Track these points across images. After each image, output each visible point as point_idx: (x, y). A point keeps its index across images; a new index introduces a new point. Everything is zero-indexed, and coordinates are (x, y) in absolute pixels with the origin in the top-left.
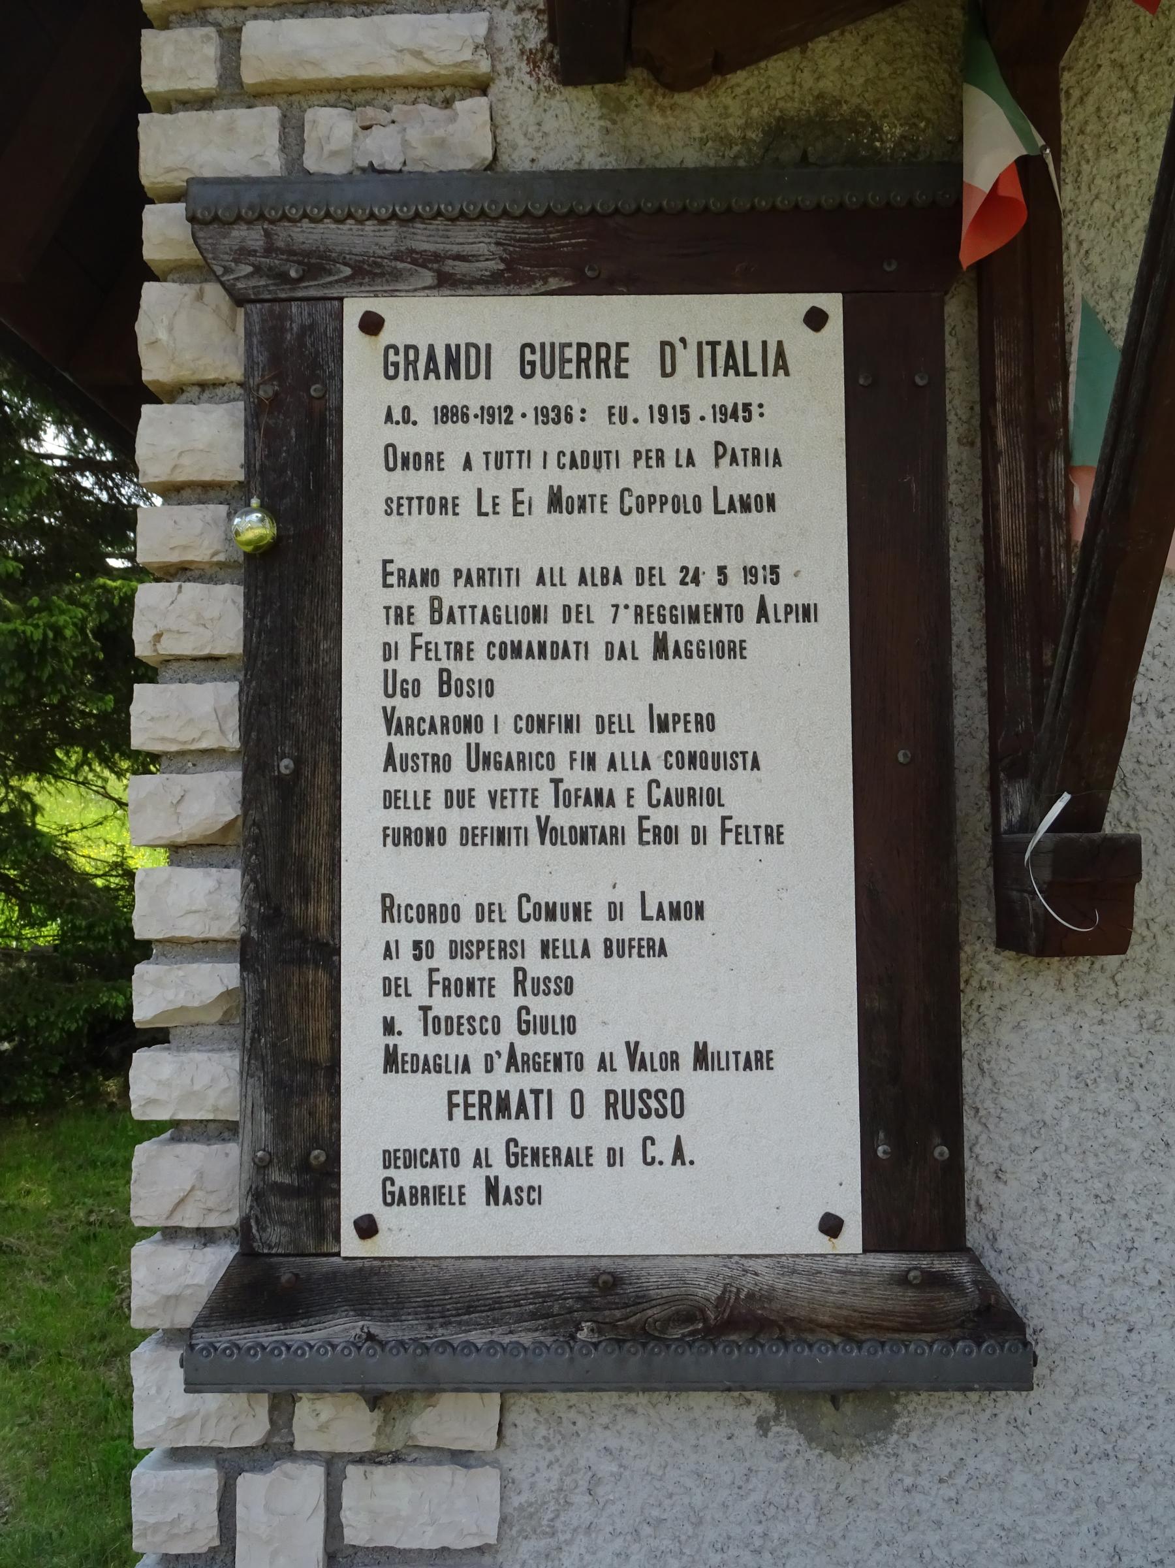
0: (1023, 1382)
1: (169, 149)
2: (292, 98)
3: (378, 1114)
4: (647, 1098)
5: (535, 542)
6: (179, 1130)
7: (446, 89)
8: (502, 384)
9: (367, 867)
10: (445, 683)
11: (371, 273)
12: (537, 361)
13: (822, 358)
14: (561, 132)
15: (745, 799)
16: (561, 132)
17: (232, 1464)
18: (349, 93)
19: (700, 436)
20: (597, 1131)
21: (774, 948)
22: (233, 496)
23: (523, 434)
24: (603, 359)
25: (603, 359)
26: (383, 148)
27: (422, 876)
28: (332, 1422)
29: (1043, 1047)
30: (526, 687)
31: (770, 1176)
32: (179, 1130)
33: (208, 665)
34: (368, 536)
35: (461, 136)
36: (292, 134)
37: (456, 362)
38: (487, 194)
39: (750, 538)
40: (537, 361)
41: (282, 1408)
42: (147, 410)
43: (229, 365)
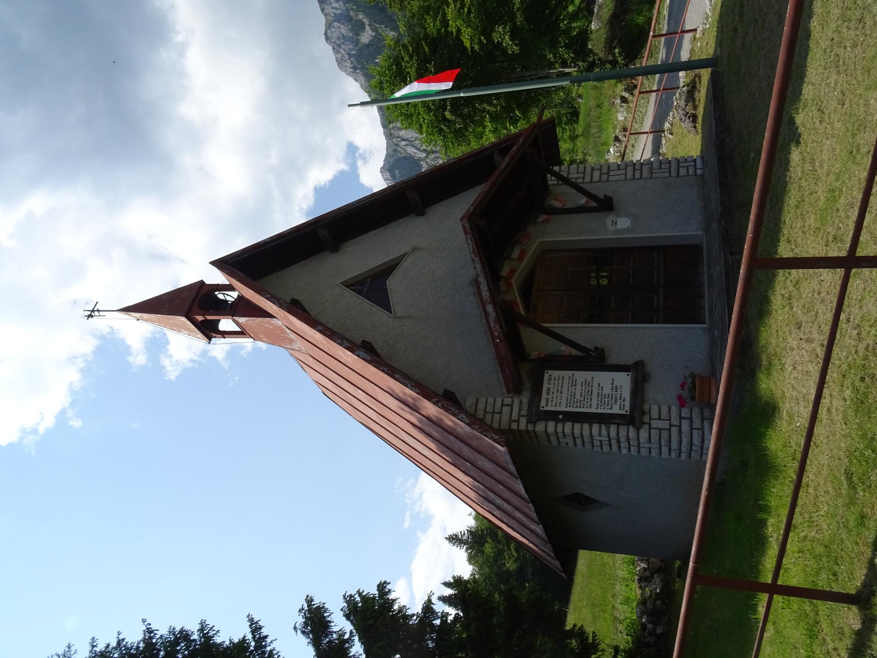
0: (642, 361)
1: (523, 425)
2: (519, 416)
3: (616, 410)
5: (565, 395)
7: (521, 402)
8: (550, 397)
9: (593, 410)
12: (548, 394)
13: (550, 372)
15: (589, 379)
17: (650, 428)
18: (520, 410)
20: (619, 393)
21: (603, 379)
23: (555, 396)
24: (549, 389)
25: (549, 389)
26: (525, 408)
28: (646, 419)
30: (578, 396)
31: (624, 380)
35: (525, 400)
37: (547, 400)
39: (566, 379)
40: (548, 394)
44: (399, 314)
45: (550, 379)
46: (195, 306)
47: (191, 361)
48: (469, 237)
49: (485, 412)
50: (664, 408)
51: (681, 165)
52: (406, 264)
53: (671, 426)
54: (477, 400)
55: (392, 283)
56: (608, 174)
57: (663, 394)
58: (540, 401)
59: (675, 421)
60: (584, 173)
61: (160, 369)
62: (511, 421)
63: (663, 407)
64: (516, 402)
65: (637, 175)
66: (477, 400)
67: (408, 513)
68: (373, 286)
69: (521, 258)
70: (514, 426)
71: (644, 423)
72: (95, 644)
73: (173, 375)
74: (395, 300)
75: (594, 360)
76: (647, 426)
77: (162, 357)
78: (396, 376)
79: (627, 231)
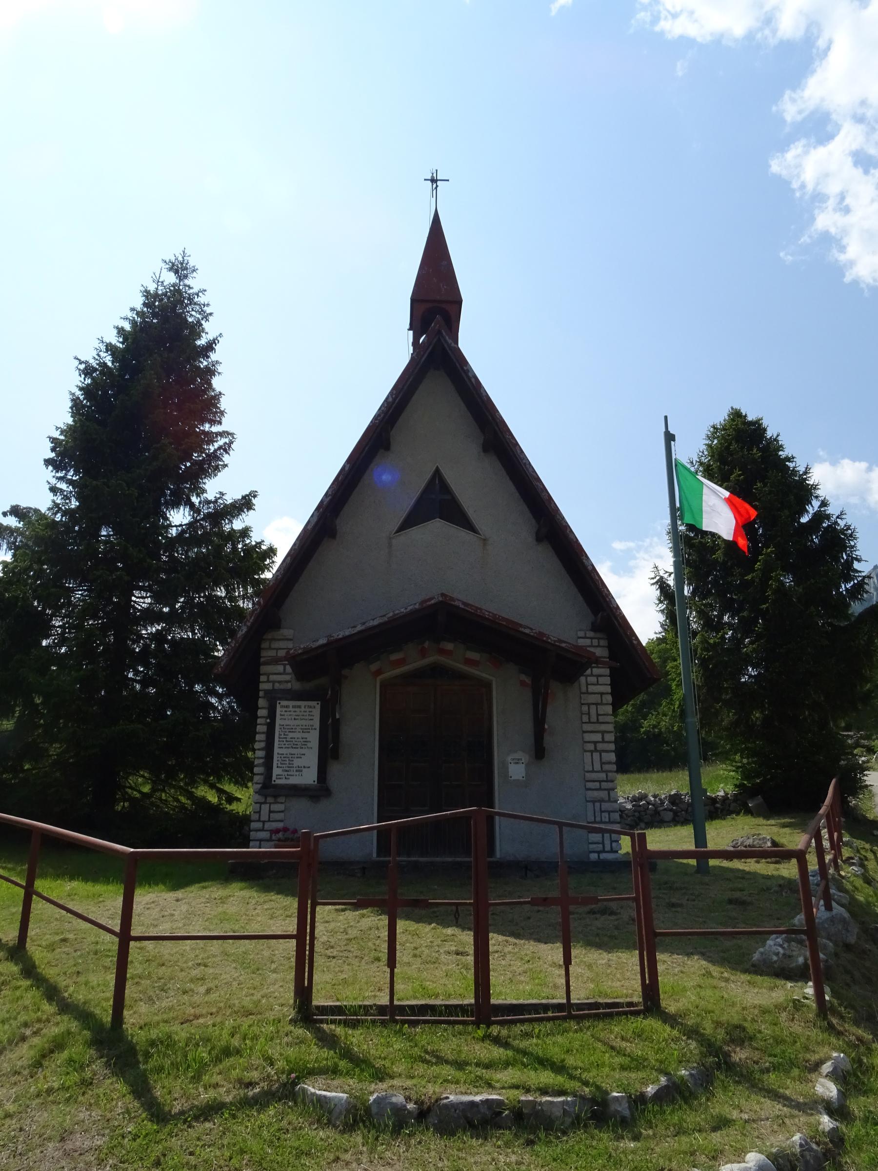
1: (263, 686)
2: (274, 682)
3: (276, 771)
4: (299, 770)
6: (258, 774)
7: (287, 682)
9: (276, 750)
10: (392, 1015)
11: (280, 699)
13: (318, 707)
14: (297, 686)
15: (309, 745)
16: (297, 686)
17: (261, 803)
18: (279, 682)
19: (307, 713)
20: (295, 773)
22: (267, 718)
24: (299, 707)
25: (299, 707)
26: (282, 687)
27: (281, 751)
28: (270, 800)
29: (335, 768)
30: (291, 735)
31: (310, 777)
32: (258, 774)
33: (263, 733)
34: (278, 722)
35: (289, 686)
36: (273, 686)
37: (287, 707)
38: (288, 691)
39: (311, 723)
40: (293, 707)
41: (266, 799)
42: (295, 933)
43: (266, 706)
44: (394, 541)
45: (310, 707)
46: (436, 302)
47: (803, 186)
48: (417, 606)
49: (277, 649)
50: (280, 816)
51: (607, 836)
52: (463, 534)
53: (264, 822)
54: (291, 640)
55: (437, 526)
56: (596, 750)
57: (300, 816)
58: (287, 700)
59: (268, 826)
60: (598, 722)
61: (783, 146)
62: (268, 675)
63: (282, 815)
64: (288, 678)
65: (590, 785)
66: (291, 640)
67: (632, 544)
68: (438, 503)
69: (469, 662)
70: (263, 678)
71: (266, 797)
72: (200, 294)
73: (775, 167)
74: (417, 533)
75: (330, 750)
76: (263, 800)
77: (803, 142)
78: (289, 558)
79: (505, 774)
